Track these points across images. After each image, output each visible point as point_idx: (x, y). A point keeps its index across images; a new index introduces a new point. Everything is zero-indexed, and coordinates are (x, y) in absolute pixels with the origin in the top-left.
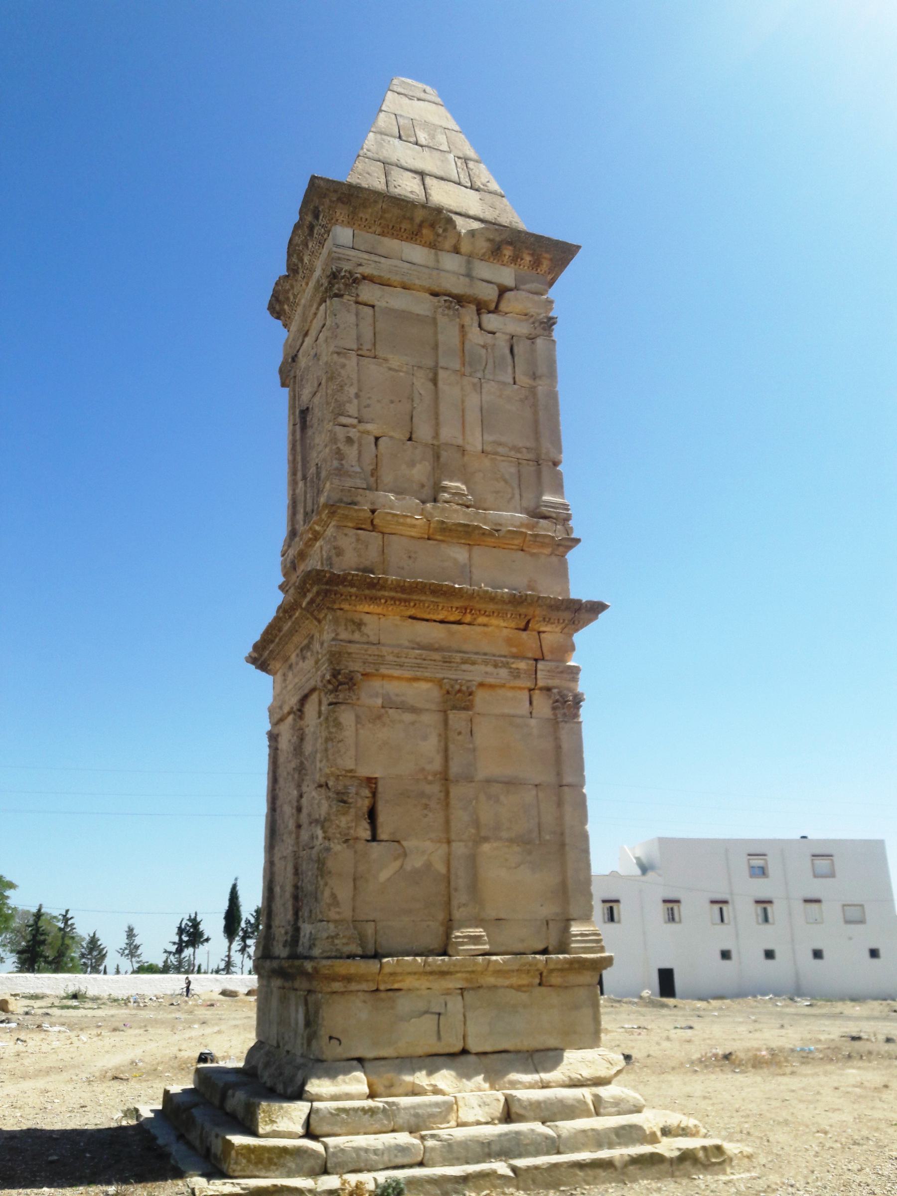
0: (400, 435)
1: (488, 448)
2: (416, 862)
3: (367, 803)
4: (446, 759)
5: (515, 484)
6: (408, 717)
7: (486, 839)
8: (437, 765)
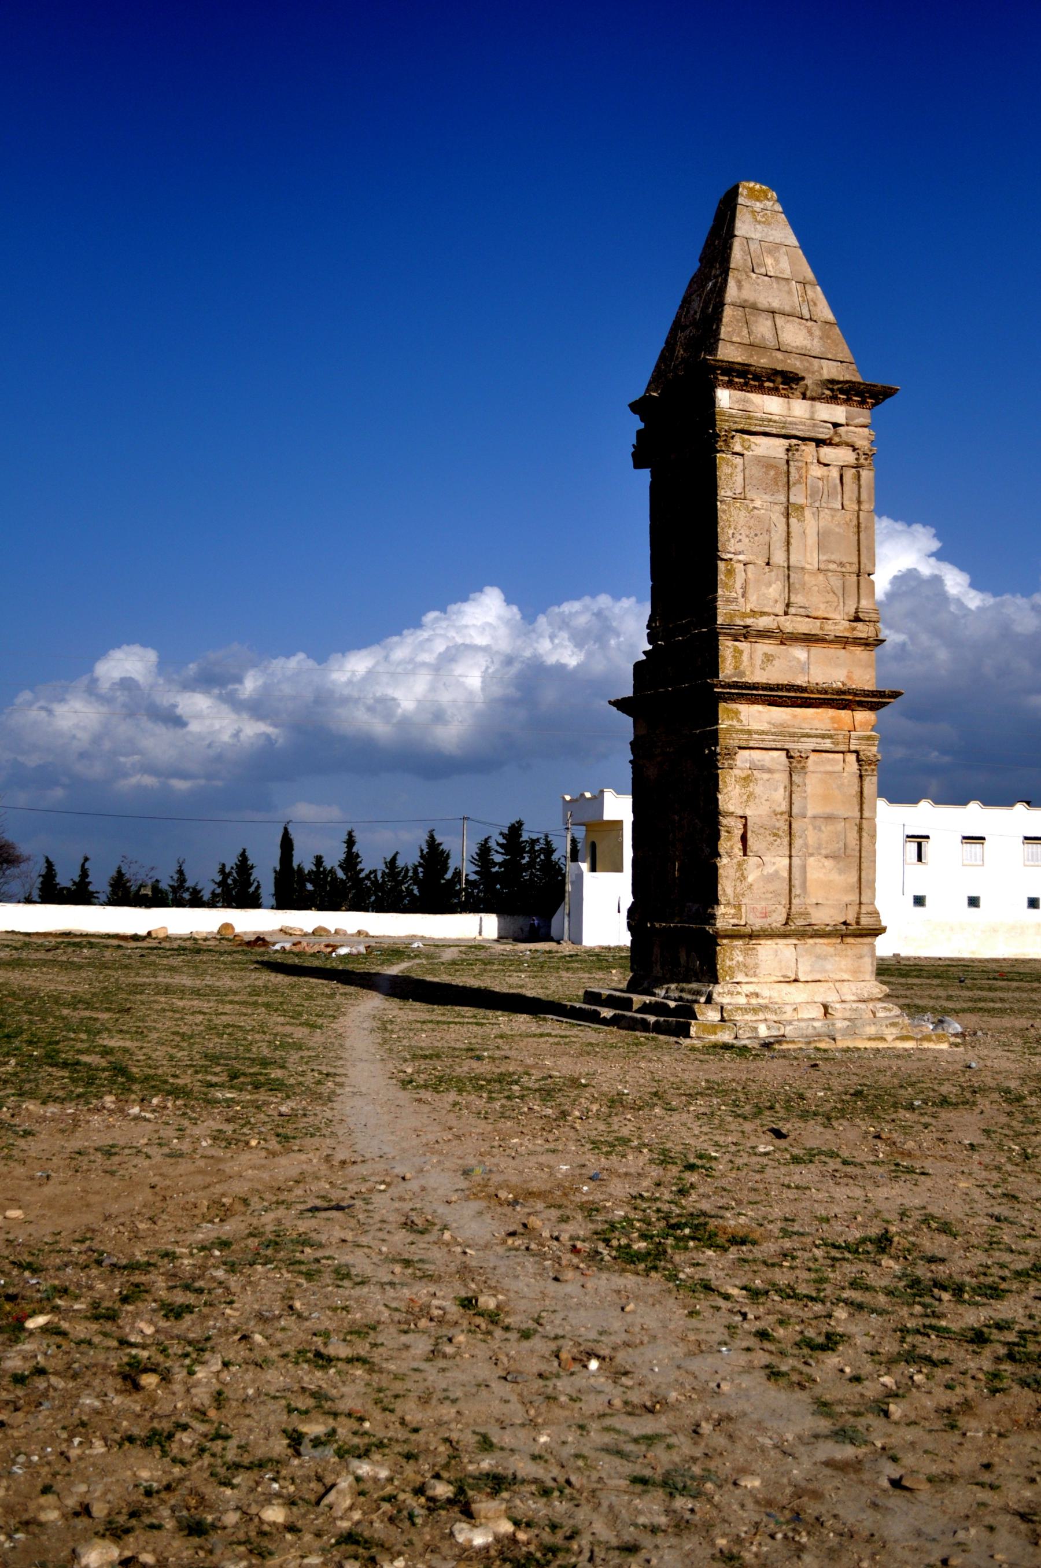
0: (761, 562)
1: (822, 567)
2: (770, 870)
3: (741, 832)
4: (791, 804)
5: (840, 593)
6: (766, 776)
7: (811, 855)
8: (784, 807)
